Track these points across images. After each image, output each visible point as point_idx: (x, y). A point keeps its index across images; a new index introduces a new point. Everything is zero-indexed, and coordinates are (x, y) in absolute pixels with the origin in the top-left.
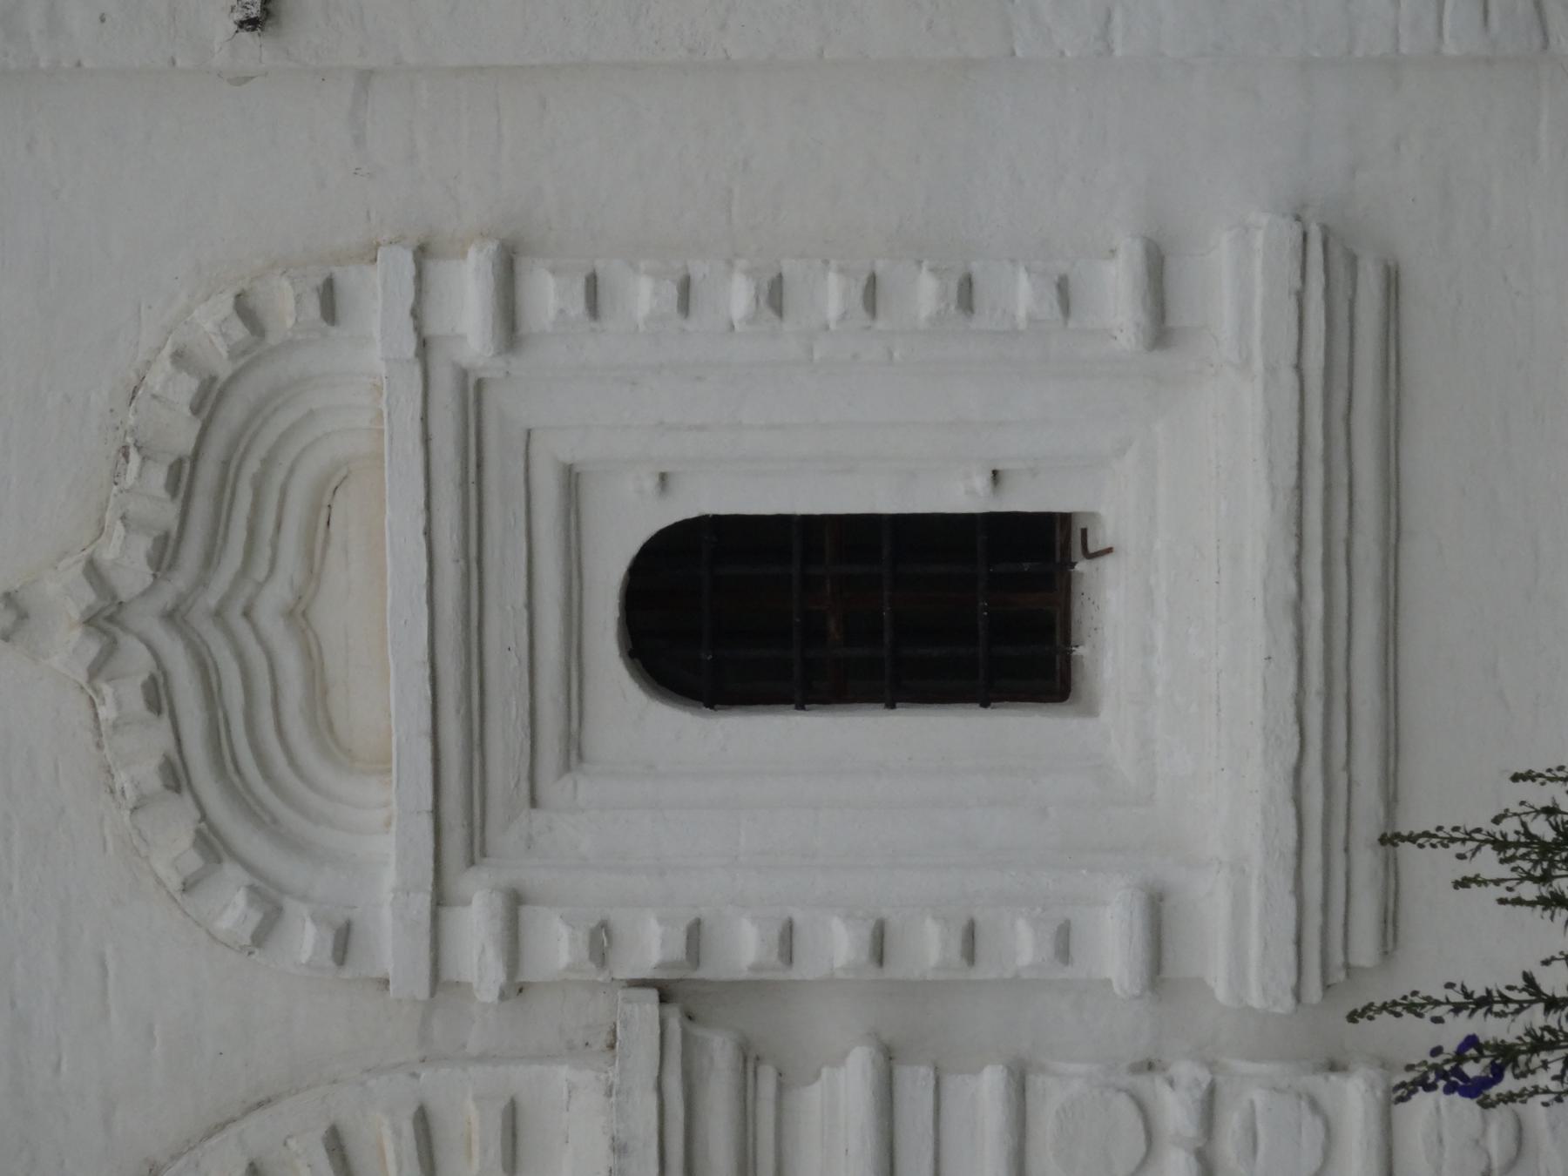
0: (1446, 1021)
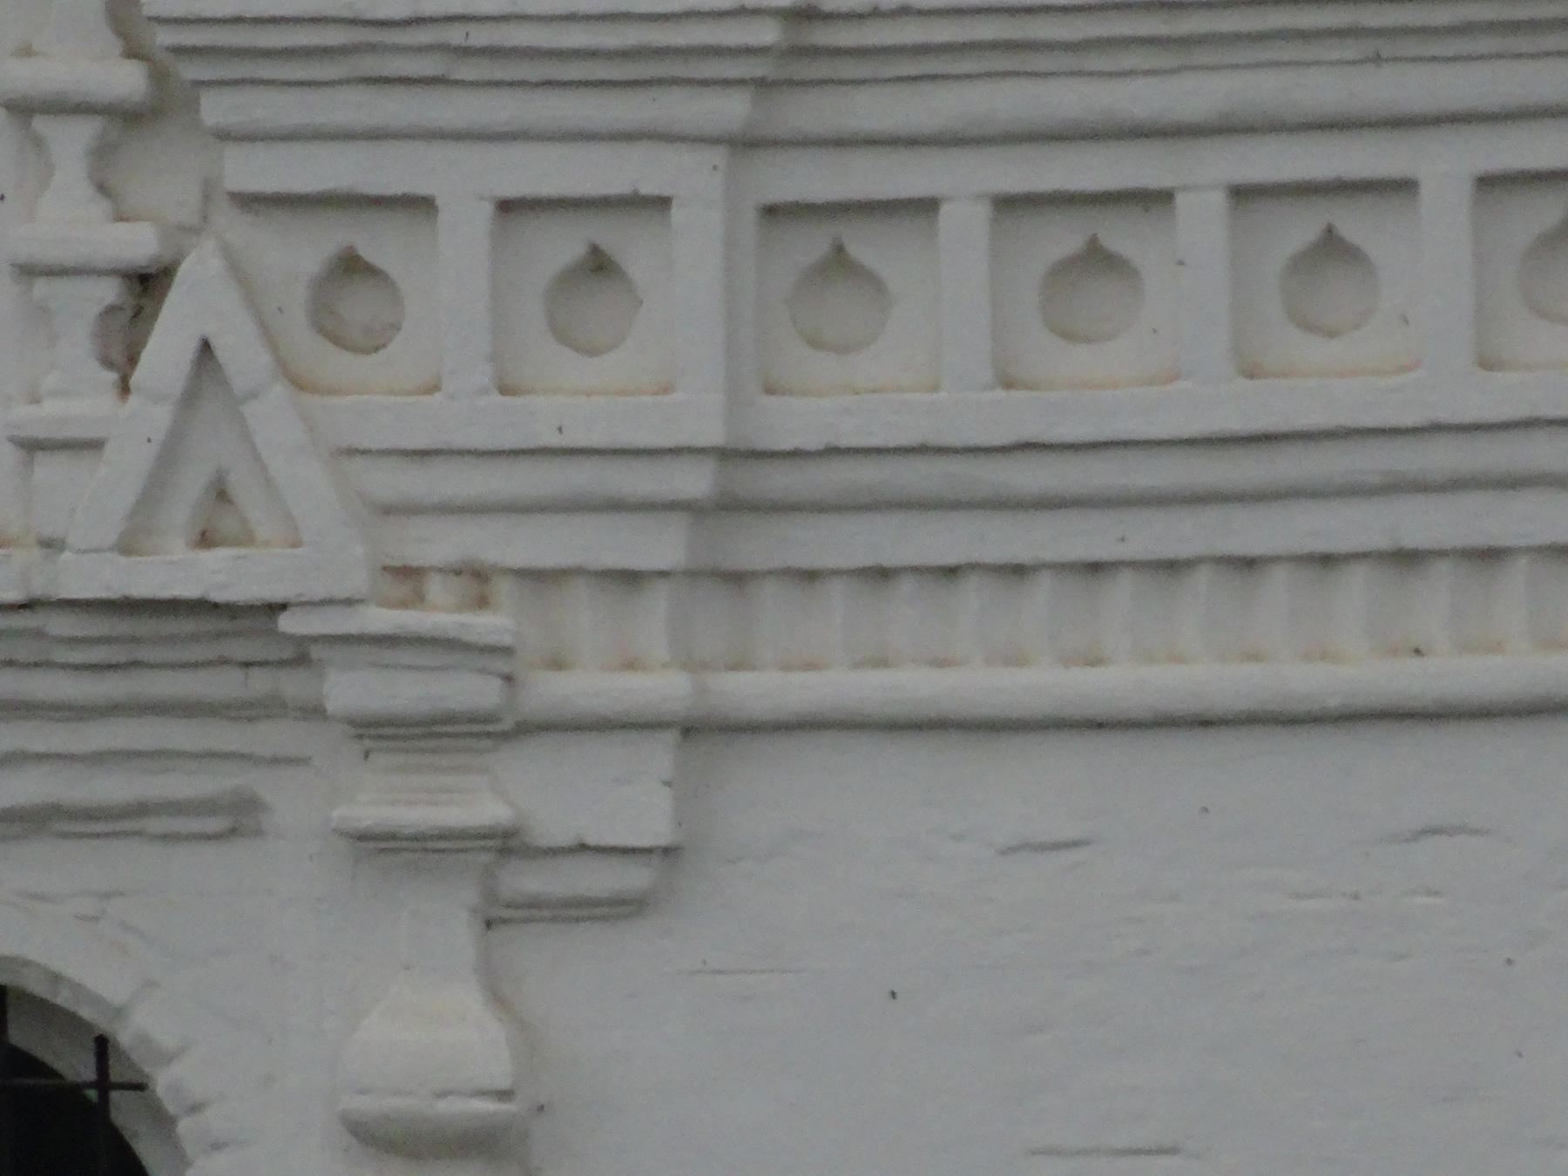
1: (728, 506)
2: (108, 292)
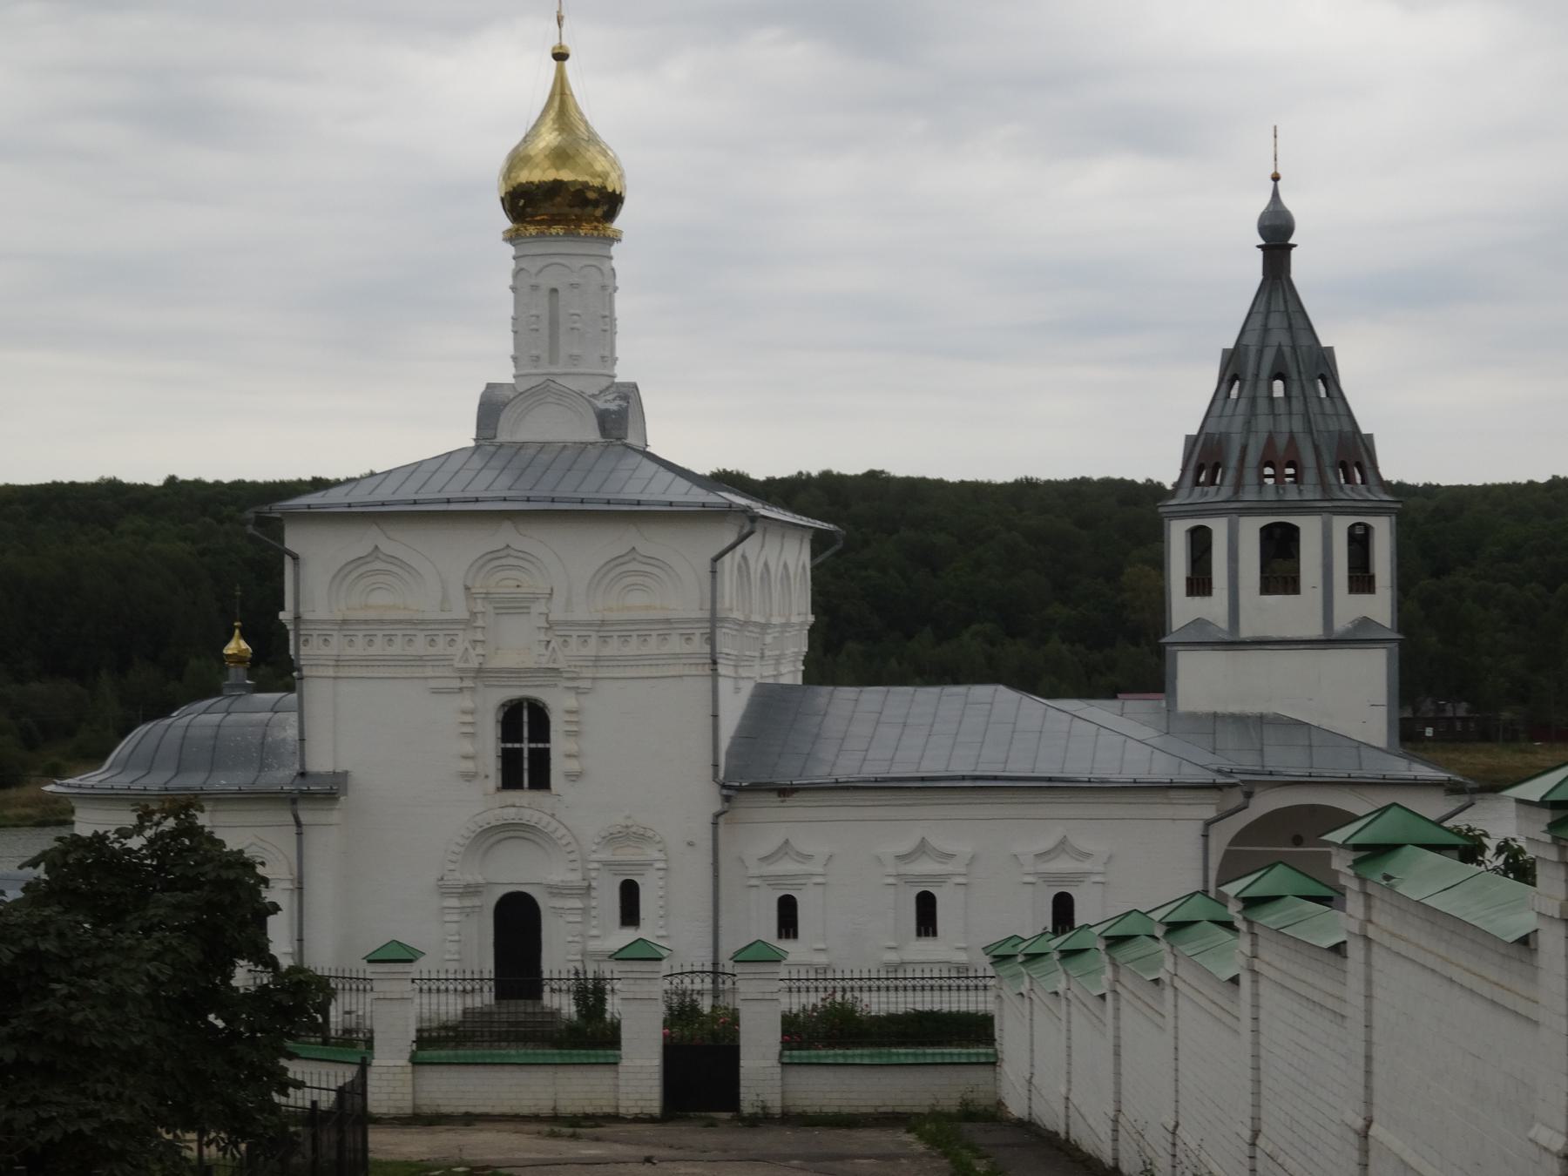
0: (1540, 879)
1: (596, 661)
2: (545, 643)
